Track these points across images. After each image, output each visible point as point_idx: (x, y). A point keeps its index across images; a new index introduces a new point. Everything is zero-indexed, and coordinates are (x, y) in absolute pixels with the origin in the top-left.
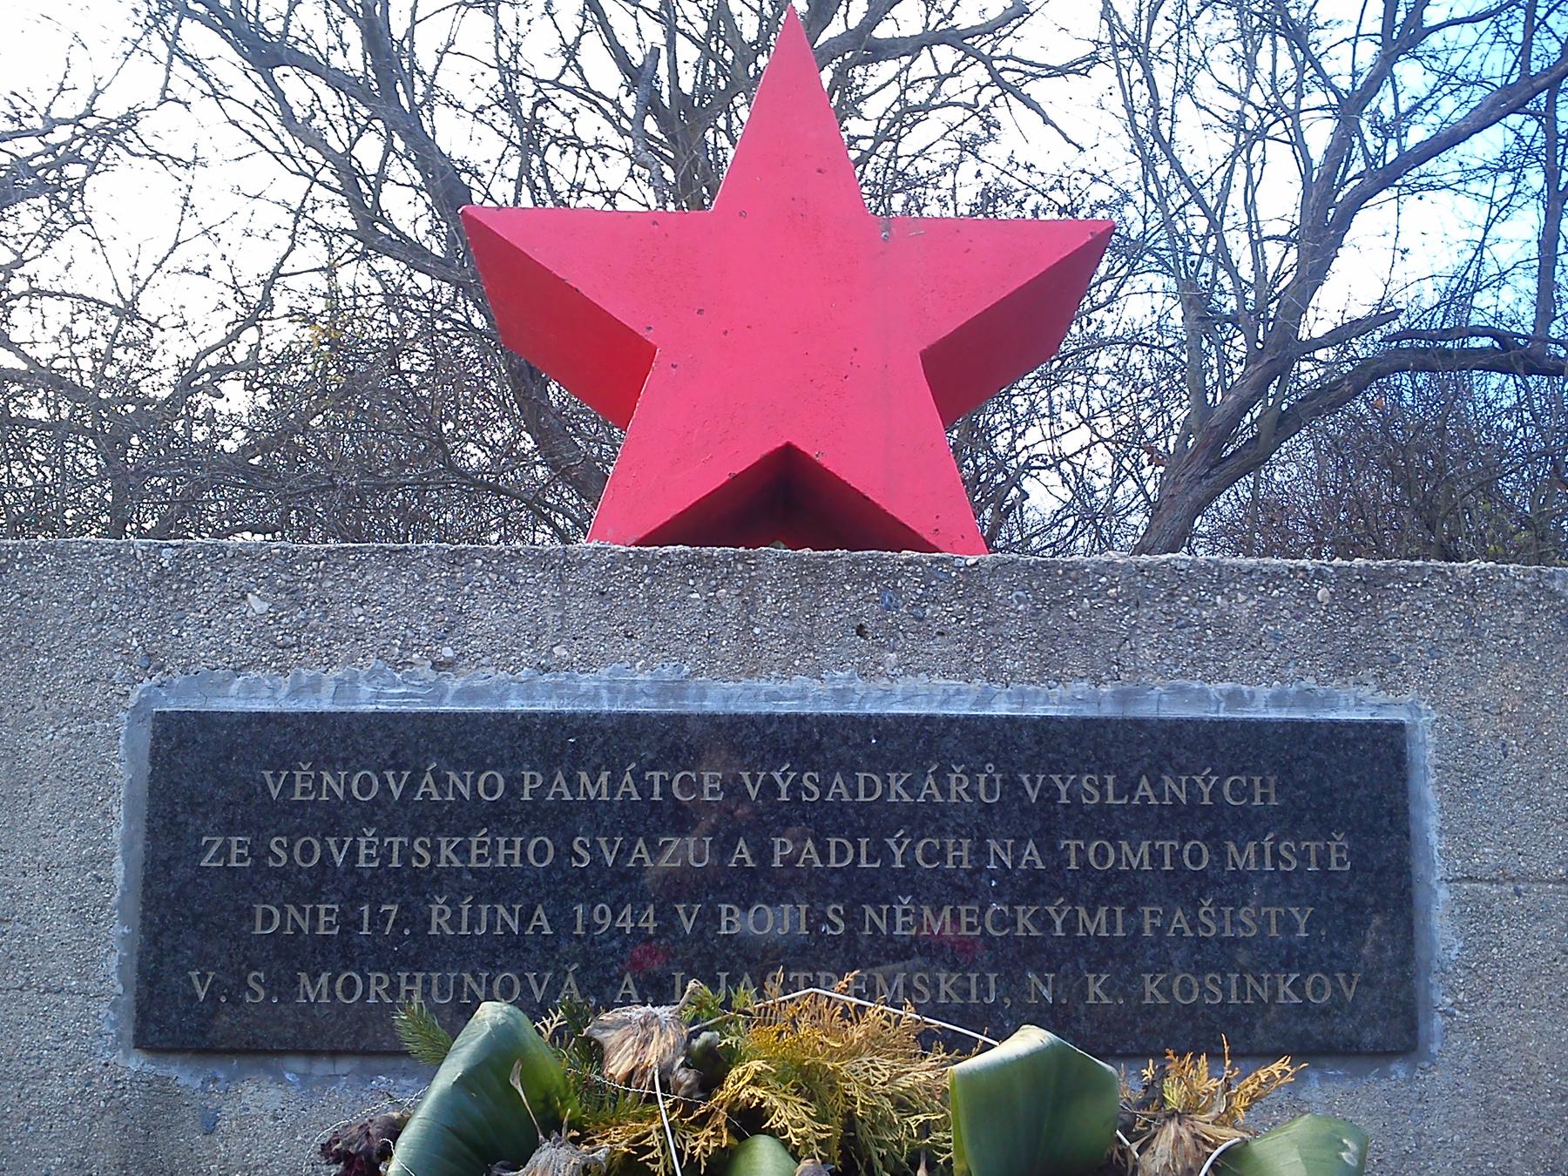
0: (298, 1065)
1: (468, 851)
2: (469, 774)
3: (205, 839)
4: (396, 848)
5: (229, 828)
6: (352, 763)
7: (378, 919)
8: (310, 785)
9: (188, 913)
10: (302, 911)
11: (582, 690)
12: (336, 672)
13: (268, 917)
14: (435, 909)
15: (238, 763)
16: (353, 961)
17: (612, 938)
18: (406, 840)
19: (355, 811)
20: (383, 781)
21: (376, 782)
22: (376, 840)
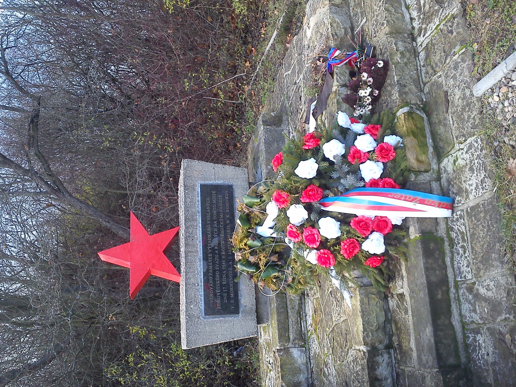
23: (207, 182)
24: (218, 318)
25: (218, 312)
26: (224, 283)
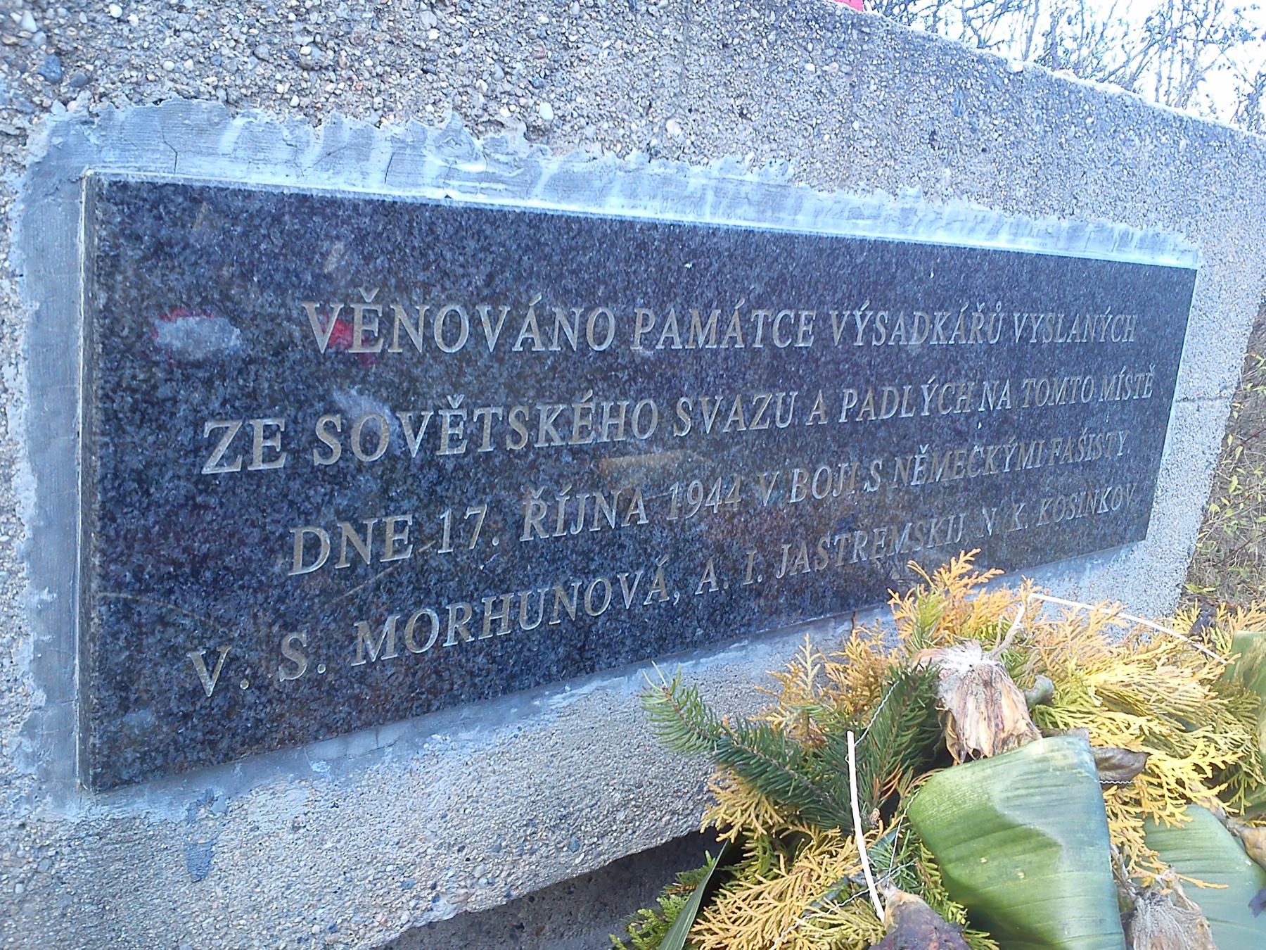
0: (331, 748)
1: (569, 423)
2: (578, 311)
3: (209, 426)
4: (488, 422)
5: (249, 406)
6: (435, 292)
7: (462, 526)
8: (375, 327)
9: (183, 558)
10: (361, 529)
11: (690, 188)
12: (393, 127)
13: (313, 546)
14: (530, 505)
15: (262, 287)
16: (428, 592)
17: (701, 520)
18: (500, 411)
19: (437, 370)
20: (475, 321)
21: (466, 323)
22: (463, 413)
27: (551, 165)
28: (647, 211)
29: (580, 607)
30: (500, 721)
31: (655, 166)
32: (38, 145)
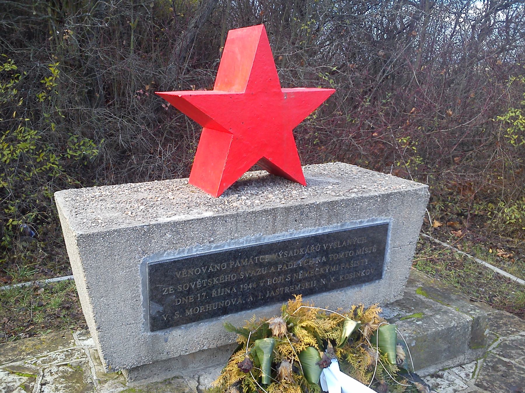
0: (185, 325)
2: (219, 265)
10: (186, 298)
12: (188, 247)
20: (201, 269)
23: (390, 233)
24: (143, 292)
25: (157, 288)
26: (214, 293)
27: (214, 245)
28: (233, 247)
29: (224, 305)
30: (212, 321)
31: (233, 241)
32: (141, 262)
